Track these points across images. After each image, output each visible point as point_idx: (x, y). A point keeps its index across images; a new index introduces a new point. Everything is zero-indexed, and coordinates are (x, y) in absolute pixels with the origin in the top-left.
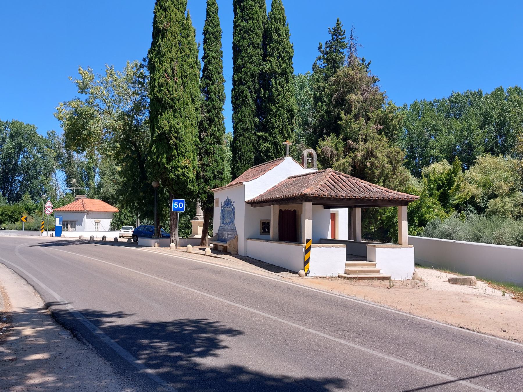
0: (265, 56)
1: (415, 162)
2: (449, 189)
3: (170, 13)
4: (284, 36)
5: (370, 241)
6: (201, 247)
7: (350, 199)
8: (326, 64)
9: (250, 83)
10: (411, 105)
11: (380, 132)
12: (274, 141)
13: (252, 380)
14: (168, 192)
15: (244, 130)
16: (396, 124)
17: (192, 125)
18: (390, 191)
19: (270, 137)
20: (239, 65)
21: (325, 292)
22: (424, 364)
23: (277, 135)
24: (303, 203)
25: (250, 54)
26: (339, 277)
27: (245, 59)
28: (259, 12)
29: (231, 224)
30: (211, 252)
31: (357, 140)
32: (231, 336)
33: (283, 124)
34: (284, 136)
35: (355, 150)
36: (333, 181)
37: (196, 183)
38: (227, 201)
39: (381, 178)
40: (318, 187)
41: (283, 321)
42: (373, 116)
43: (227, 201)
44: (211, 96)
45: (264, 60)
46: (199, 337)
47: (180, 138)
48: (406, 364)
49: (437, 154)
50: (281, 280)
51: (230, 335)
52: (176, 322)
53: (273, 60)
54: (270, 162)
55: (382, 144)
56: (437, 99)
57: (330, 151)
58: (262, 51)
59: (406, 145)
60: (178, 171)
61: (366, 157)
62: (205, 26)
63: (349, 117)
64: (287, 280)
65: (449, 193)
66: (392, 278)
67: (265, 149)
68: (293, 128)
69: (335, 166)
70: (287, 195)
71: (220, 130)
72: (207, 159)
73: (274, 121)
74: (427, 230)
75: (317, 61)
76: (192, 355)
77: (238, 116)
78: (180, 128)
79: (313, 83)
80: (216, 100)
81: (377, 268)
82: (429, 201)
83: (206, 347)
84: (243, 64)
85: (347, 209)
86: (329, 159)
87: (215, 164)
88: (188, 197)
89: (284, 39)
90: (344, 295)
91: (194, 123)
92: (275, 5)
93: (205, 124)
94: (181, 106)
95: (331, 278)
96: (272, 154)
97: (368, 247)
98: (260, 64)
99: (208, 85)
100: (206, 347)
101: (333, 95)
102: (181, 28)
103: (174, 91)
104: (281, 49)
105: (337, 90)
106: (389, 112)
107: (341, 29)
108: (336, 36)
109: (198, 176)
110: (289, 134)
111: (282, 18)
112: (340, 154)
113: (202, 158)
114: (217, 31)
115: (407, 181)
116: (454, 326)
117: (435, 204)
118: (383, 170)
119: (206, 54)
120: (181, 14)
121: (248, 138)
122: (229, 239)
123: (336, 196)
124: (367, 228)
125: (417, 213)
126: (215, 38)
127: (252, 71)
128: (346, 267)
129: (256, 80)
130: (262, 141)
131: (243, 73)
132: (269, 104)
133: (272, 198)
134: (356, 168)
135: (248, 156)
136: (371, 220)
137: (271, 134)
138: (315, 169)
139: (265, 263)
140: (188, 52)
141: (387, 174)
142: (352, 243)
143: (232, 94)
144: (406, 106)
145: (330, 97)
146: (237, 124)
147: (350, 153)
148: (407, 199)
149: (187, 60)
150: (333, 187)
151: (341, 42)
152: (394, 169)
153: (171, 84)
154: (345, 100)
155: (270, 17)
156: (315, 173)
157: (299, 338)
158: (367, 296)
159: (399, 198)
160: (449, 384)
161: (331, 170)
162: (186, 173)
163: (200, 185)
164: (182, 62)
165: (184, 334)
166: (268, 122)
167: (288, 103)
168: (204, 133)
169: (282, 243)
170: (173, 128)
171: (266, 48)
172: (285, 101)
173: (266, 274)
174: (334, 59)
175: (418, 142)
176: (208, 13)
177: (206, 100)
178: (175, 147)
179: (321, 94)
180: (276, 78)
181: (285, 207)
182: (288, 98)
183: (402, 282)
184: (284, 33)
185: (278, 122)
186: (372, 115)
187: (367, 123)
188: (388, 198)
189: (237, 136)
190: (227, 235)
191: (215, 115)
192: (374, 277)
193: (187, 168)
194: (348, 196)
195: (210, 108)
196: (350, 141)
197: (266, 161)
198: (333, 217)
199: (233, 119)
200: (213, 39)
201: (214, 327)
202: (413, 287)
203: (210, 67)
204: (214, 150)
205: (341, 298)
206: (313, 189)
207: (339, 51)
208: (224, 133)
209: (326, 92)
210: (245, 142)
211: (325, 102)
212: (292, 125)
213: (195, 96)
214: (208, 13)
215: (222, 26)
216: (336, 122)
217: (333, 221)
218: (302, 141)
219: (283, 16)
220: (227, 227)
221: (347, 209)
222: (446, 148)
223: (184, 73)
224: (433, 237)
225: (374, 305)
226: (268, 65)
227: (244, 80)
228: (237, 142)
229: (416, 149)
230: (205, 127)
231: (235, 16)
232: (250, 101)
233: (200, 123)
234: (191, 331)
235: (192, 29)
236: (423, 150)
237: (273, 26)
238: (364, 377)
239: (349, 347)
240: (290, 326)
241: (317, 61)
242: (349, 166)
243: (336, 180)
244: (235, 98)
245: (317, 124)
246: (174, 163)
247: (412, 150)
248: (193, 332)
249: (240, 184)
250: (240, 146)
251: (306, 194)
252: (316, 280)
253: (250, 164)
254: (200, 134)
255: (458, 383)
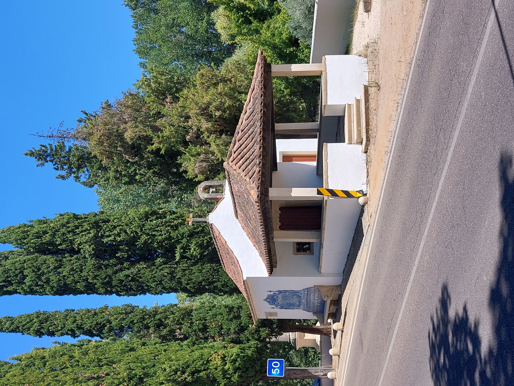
0: (73, 252)
1: (215, 51)
2: (249, 9)
3: (12, 383)
4: (47, 227)
5: (318, 108)
6: (332, 336)
7: (264, 138)
8: (85, 169)
9: (108, 270)
10: (141, 58)
11: (176, 99)
12: (188, 237)
13: (507, 279)
14: (258, 382)
15: (172, 278)
16: (165, 78)
17: (165, 351)
18: (252, 87)
19: (182, 242)
20: (84, 286)
21: (386, 171)
22: (475, 50)
23: (179, 234)
24: (270, 199)
25: (70, 272)
26: (366, 152)
27: (77, 278)
28: (13, 260)
29: (300, 295)
30: (339, 322)
31: (186, 128)
32: (450, 300)
33: (164, 226)
34: (181, 224)
35: (200, 131)
36: (240, 160)
37: (245, 344)
38: (268, 300)
39: (235, 97)
40: (248, 180)
41: (427, 230)
42: (154, 108)
43: (268, 300)
44: (126, 325)
45: (78, 252)
46: (452, 345)
47: (183, 368)
48: (476, 73)
49: (205, 24)
50: (373, 228)
51: (448, 302)
52: (434, 376)
53: (78, 240)
54: (216, 242)
55: (191, 96)
56: (132, 24)
57: (201, 164)
58: (66, 255)
59: (193, 63)
60: (229, 369)
61: (209, 117)
62: (31, 335)
63: (155, 139)
64: (372, 220)
65: (254, 10)
66: (366, 84)
67: (197, 250)
68: (170, 212)
69: (221, 156)
70: (260, 221)
71: (172, 312)
72: (212, 328)
73: (160, 238)
74: (303, 37)
75: (81, 181)
76: (477, 356)
77: (153, 286)
78: (170, 367)
79: (110, 185)
80: (131, 318)
81: (354, 103)
82: (266, 34)
83: (465, 337)
84: (84, 281)
85: (277, 141)
86: (212, 165)
87: (219, 317)
88: (264, 354)
89: (51, 226)
90: (390, 146)
91: (163, 348)
92: (4, 238)
93: (165, 332)
94: (140, 367)
95: (367, 162)
96: (206, 239)
97: (327, 113)
98: (83, 258)
99: (111, 329)
100: (465, 337)
101: (126, 160)
102: (33, 368)
103: (119, 377)
104: (63, 230)
105: (120, 154)
106: (148, 87)
107: (38, 151)
108: (47, 156)
109: (236, 342)
110: (178, 217)
111: (22, 229)
112: (205, 150)
113: (211, 336)
114: (38, 317)
115: (239, 64)
116: (425, 8)
117: (269, 27)
118: (226, 95)
119: (69, 332)
120: (14, 369)
121: (183, 272)
122: (320, 296)
123: (260, 157)
124: (301, 114)
125: (280, 49)
126: (46, 320)
127: (92, 268)
128: (353, 143)
129: (104, 263)
130: (188, 254)
131: (95, 281)
132: (138, 245)
133: (263, 240)
134: (223, 130)
135: (208, 272)
136: (290, 109)
137: (178, 242)
138: (225, 182)
139: (352, 249)
140: (66, 358)
141: (231, 89)
142: (321, 134)
143: (124, 295)
144: (141, 63)
145: (128, 165)
146: (164, 288)
147: (203, 137)
148: (263, 65)
149: (77, 359)
150: (248, 161)
151: (56, 150)
152: (224, 81)
153: (109, 381)
154: (133, 144)
155: (20, 245)
156: (230, 184)
157: (448, 209)
158: (391, 117)
159: (261, 76)
160: (501, 19)
161: (226, 163)
162: (232, 358)
163: (248, 338)
164: (79, 366)
165: (450, 366)
166: (162, 246)
167: (136, 219)
168: (177, 334)
169: (323, 226)
170: (170, 376)
171: (62, 250)
172: (133, 223)
173: (365, 248)
174: (78, 159)
175: (189, 48)
176: (13, 331)
177: (132, 331)
178: (196, 374)
179: (125, 176)
180: (102, 236)
181: (276, 222)
182: (129, 219)
183: (371, 70)
184: (42, 226)
185: (161, 232)
186: (153, 109)
187: (163, 116)
188: (262, 89)
189: (180, 287)
190: (315, 300)
191: (152, 319)
192: (365, 107)
193: (225, 357)
194: (260, 141)
195: (142, 326)
196: (188, 137)
197: (215, 247)
198: (287, 158)
199: (158, 294)
200: (48, 323)
201: (439, 324)
202: (376, 57)
203: (86, 327)
204: (200, 319)
205: (394, 151)
206: (251, 187)
207: (67, 152)
208: (176, 305)
209: (122, 169)
210: (188, 277)
211: (135, 170)
212: (166, 213)
213: (127, 347)
214: (12, 330)
215: (32, 310)
216: (162, 156)
217: (293, 158)
218: (187, 198)
219: (20, 228)
220: (304, 301)
221: (277, 141)
222: (197, 13)
223: (95, 363)
224: (312, 29)
225: (401, 109)
226: (84, 246)
227: (105, 279)
228: (188, 287)
229: (198, 51)
230: (168, 332)
231: (17, 293)
232: (134, 270)
233: (163, 340)
234: (446, 356)
235: (34, 353)
236: (199, 42)
237: (32, 241)
238: (497, 127)
239: (458, 145)
240: (433, 220)
241: (81, 181)
242: (220, 138)
243: (239, 156)
244: (129, 291)
245: (165, 180)
246: (219, 374)
247: (199, 56)
248: (447, 352)
249: (246, 284)
250: (195, 283)
251: (258, 196)
252: (372, 182)
253: (219, 269)
254: (178, 339)
255: (499, 8)
